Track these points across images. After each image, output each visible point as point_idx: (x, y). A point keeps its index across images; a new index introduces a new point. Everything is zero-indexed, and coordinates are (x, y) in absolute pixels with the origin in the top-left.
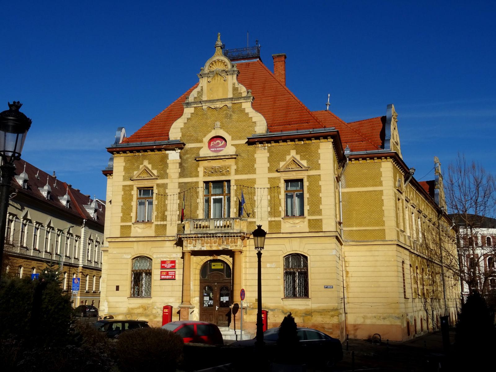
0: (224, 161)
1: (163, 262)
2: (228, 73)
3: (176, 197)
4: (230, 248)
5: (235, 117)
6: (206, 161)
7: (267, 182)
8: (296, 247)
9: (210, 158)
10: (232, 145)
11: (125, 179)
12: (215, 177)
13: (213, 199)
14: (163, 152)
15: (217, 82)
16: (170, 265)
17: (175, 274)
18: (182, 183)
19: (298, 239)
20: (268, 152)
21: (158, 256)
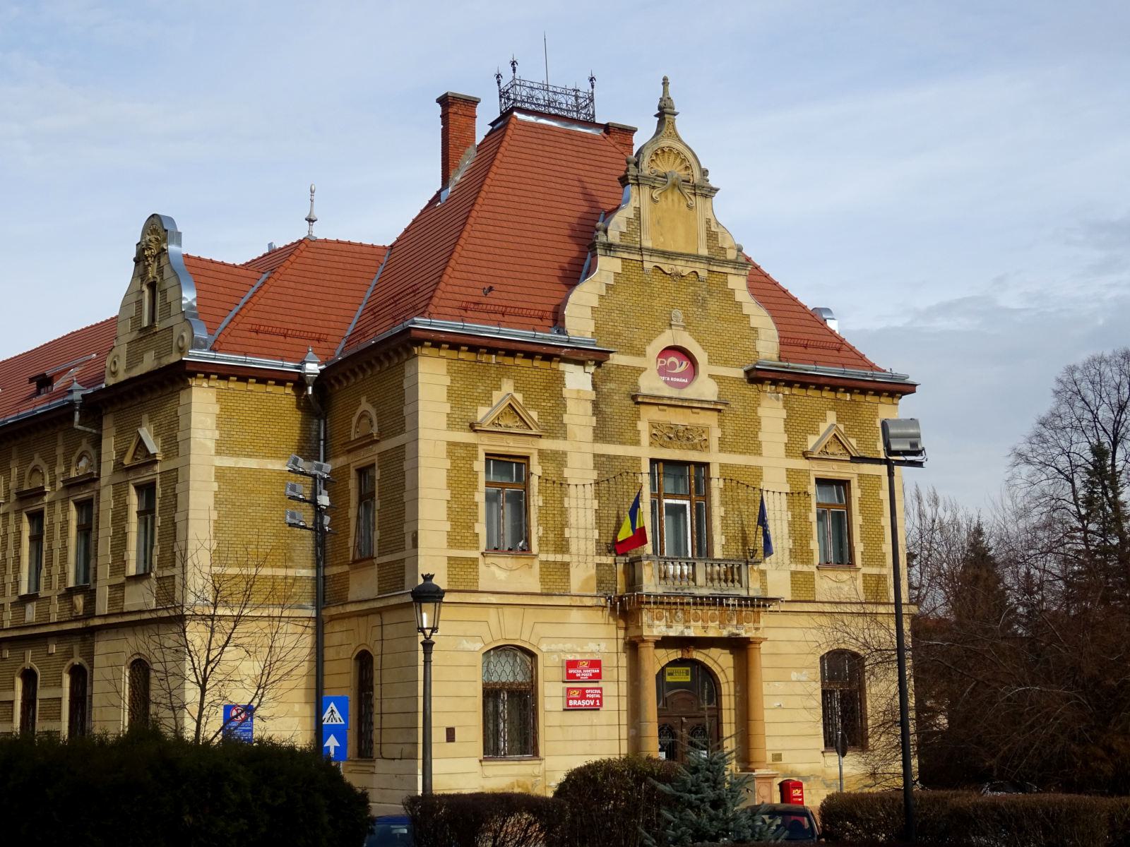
0: (695, 413)
1: (572, 664)
2: (698, 191)
3: (590, 491)
4: (744, 635)
5: (713, 305)
6: (656, 408)
7: (785, 479)
8: (514, 628)
9: (668, 402)
10: (711, 376)
11: (452, 425)
12: (677, 451)
13: (685, 506)
14: (554, 365)
15: (673, 205)
16: (589, 672)
17: (601, 695)
18: (603, 456)
19: (519, 610)
20: (785, 407)
21: (553, 647)
